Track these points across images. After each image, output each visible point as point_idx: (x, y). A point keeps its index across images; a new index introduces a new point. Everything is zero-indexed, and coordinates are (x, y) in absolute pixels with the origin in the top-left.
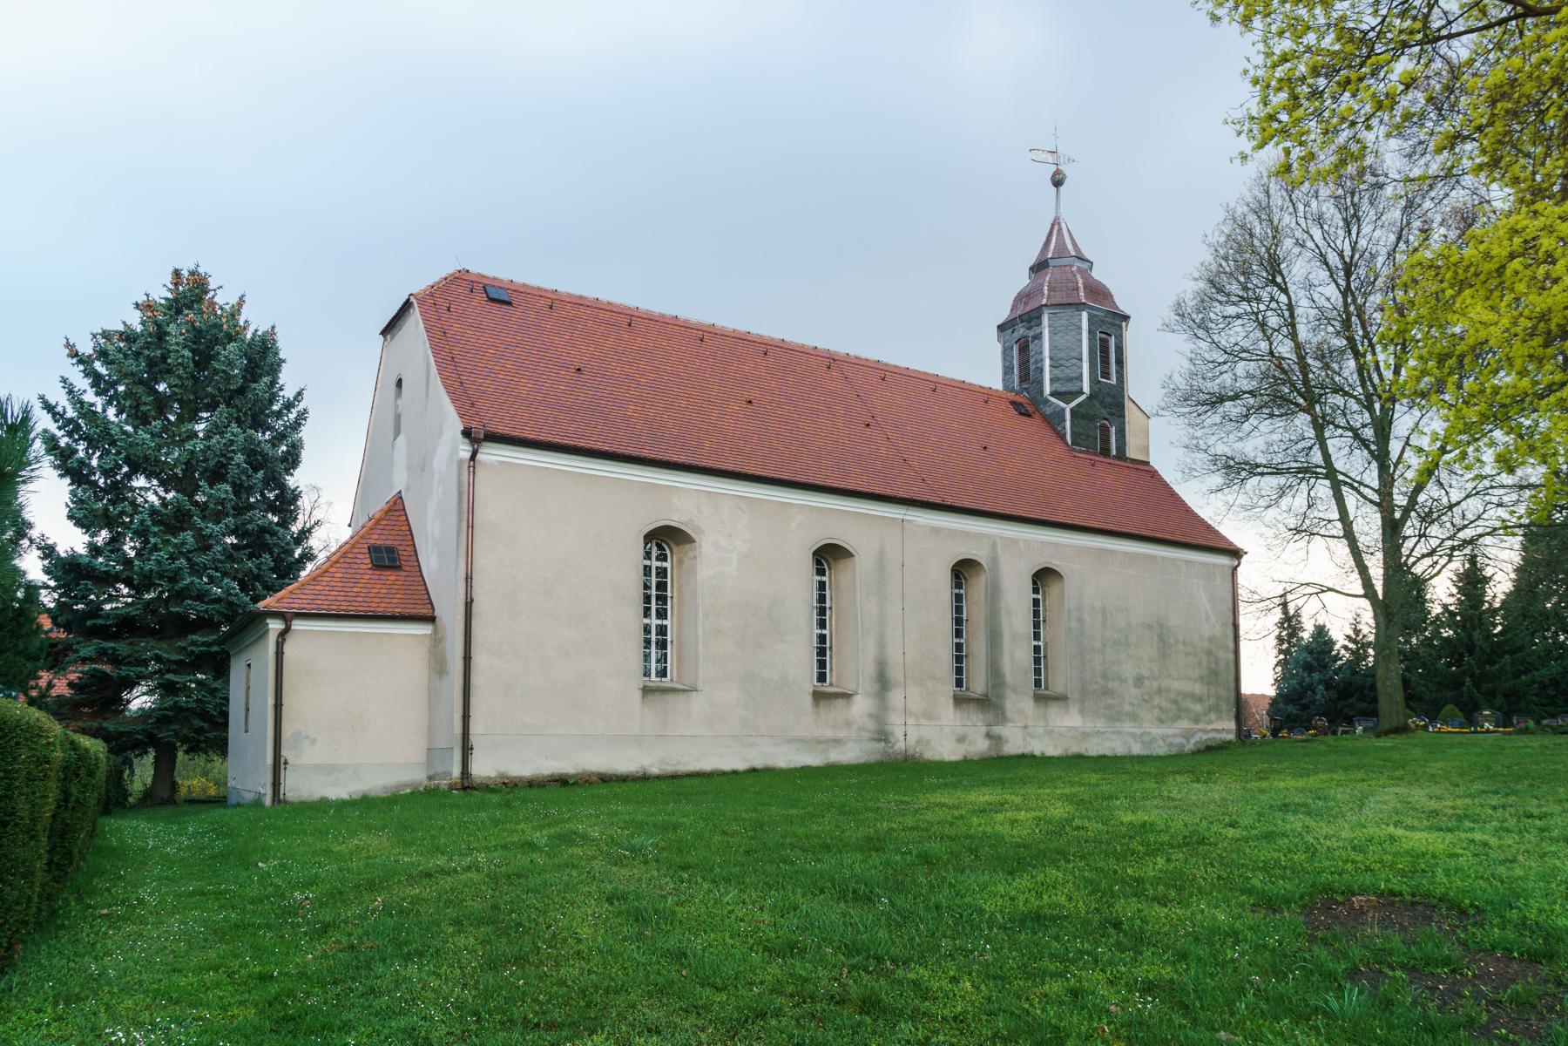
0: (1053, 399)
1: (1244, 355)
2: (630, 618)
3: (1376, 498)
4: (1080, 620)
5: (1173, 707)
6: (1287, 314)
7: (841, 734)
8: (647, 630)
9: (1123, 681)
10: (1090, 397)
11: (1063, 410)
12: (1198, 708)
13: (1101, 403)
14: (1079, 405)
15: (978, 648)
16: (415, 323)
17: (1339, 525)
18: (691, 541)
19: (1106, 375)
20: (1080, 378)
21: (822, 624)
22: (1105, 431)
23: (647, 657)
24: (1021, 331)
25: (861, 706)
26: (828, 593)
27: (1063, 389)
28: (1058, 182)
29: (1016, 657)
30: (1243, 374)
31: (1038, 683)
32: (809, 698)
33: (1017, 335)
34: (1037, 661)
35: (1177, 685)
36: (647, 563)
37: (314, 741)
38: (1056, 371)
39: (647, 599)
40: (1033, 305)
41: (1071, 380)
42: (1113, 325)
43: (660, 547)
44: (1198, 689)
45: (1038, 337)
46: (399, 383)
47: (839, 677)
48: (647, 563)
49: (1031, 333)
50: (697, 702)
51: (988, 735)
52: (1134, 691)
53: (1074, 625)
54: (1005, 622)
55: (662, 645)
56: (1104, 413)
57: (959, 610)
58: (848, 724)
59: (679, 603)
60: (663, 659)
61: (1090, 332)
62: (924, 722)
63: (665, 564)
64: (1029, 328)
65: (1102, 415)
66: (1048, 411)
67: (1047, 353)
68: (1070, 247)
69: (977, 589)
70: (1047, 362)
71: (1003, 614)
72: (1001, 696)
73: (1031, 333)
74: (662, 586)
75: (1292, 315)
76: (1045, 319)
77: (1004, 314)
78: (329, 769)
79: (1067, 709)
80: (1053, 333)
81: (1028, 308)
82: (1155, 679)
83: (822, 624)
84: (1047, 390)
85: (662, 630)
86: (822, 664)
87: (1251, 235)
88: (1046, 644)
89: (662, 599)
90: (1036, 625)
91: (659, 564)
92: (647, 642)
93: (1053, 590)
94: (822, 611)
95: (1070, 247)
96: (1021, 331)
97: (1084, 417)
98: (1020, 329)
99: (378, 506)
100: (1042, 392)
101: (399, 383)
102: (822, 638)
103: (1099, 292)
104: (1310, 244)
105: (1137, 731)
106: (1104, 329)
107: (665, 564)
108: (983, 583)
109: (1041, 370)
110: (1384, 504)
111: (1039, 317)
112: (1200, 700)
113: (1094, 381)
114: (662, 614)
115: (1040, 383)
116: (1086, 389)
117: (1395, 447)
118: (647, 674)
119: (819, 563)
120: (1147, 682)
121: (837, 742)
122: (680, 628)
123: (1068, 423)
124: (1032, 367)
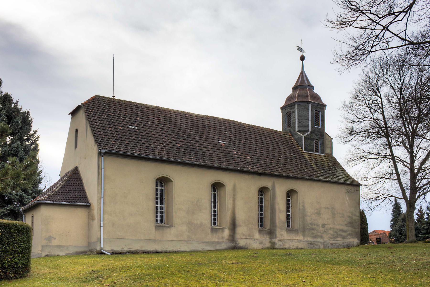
0: (298, 133)
1: (365, 119)
2: (151, 204)
3: (408, 165)
4: (303, 206)
5: (335, 234)
6: (380, 105)
7: (220, 241)
8: (157, 208)
9: (318, 225)
10: (312, 132)
11: (302, 137)
12: (344, 234)
13: (316, 134)
14: (308, 135)
15: (267, 215)
16: (82, 114)
17: (395, 175)
18: (172, 181)
19: (317, 125)
20: (308, 126)
21: (215, 207)
22: (317, 144)
23: (157, 216)
24: (288, 110)
25: (227, 233)
26: (217, 197)
27: (302, 130)
28: (302, 58)
29: (281, 216)
30: (365, 125)
31: (288, 226)
32: (210, 230)
33: (287, 111)
34: (288, 219)
35: (338, 227)
36: (157, 188)
37: (55, 239)
38: (300, 124)
39: (157, 199)
40: (293, 101)
41: (305, 126)
42: (320, 108)
43: (161, 183)
44: (345, 228)
45: (294, 112)
46: (77, 131)
47: (220, 224)
48: (157, 188)
49: (292, 111)
50: (173, 231)
51: (270, 242)
52: (322, 229)
53: (301, 208)
54: (277, 207)
55: (162, 212)
56: (317, 137)
57: (262, 203)
58: (223, 238)
59: (167, 200)
60: (162, 217)
61: (312, 111)
62: (248, 237)
63: (215, 193)
64: (291, 109)
65: (319, 139)
66: (296, 137)
67: (297, 118)
68: (306, 82)
69: (267, 197)
70: (297, 120)
71: (276, 204)
72: (275, 230)
73: (292, 111)
74: (162, 195)
75: (382, 106)
76: (296, 106)
77: (283, 103)
78: (59, 247)
79: (298, 233)
80: (299, 111)
81: (291, 102)
82: (329, 225)
83: (215, 207)
84: (297, 130)
85: (162, 208)
86: (215, 219)
87: (370, 78)
88: (292, 214)
89: (162, 199)
90: (288, 208)
91: (161, 188)
92: (157, 212)
93: (295, 197)
94: (215, 203)
95: (306, 82)
96: (288, 110)
97: (309, 139)
98: (287, 109)
99: (70, 168)
100: (295, 131)
101: (77, 131)
102: (215, 211)
103: (316, 97)
104: (388, 82)
105: (322, 241)
106: (317, 109)
107: (215, 193)
108: (270, 194)
109: (295, 123)
110: (412, 169)
111: (294, 105)
112: (345, 231)
113: (313, 127)
114: (162, 203)
115: (294, 127)
116: (310, 129)
117: (415, 150)
118: (157, 221)
119: (214, 188)
120: (326, 226)
121: (219, 243)
122: (167, 208)
123: (303, 141)
124: (292, 122)
